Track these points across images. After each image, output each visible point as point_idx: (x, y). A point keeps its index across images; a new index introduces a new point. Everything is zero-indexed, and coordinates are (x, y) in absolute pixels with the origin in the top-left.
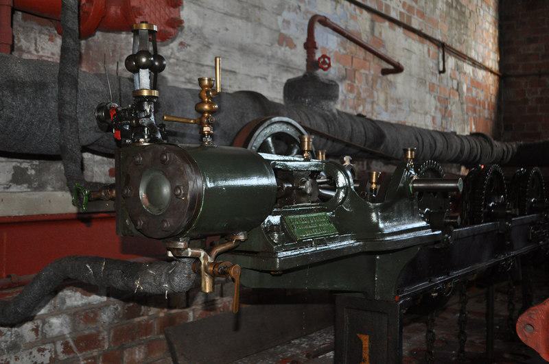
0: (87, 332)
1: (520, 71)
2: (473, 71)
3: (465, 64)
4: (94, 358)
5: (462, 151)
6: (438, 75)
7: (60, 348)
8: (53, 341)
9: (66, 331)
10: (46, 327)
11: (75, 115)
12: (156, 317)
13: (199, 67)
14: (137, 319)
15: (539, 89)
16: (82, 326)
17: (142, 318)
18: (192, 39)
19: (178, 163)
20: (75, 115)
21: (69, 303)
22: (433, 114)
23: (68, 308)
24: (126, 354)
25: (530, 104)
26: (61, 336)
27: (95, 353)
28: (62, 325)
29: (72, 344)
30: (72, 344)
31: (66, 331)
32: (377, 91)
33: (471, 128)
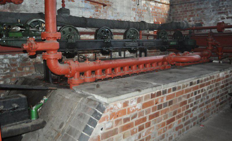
0: (13, 63)
1: (176, 3)
2: (155, 4)
3: (151, 2)
4: (16, 68)
5: (183, 27)
6: (137, 6)
7: (7, 65)
8: (5, 64)
9: (8, 62)
10: (3, 61)
11: (104, 72)
12: (32, 62)
13: (42, 8)
14: (27, 62)
15: (181, 8)
16: (12, 62)
17: (27, 62)
18: (39, 2)
19: (188, 21)
20: (104, 72)
21: (8, 57)
22: (134, 17)
23: (8, 58)
24: (24, 69)
25: (179, 13)
26: (7, 63)
27: (16, 67)
28: (7, 61)
29: (10, 65)
30: (10, 65)
31: (8, 62)
32: (108, 11)
33: (154, 20)
